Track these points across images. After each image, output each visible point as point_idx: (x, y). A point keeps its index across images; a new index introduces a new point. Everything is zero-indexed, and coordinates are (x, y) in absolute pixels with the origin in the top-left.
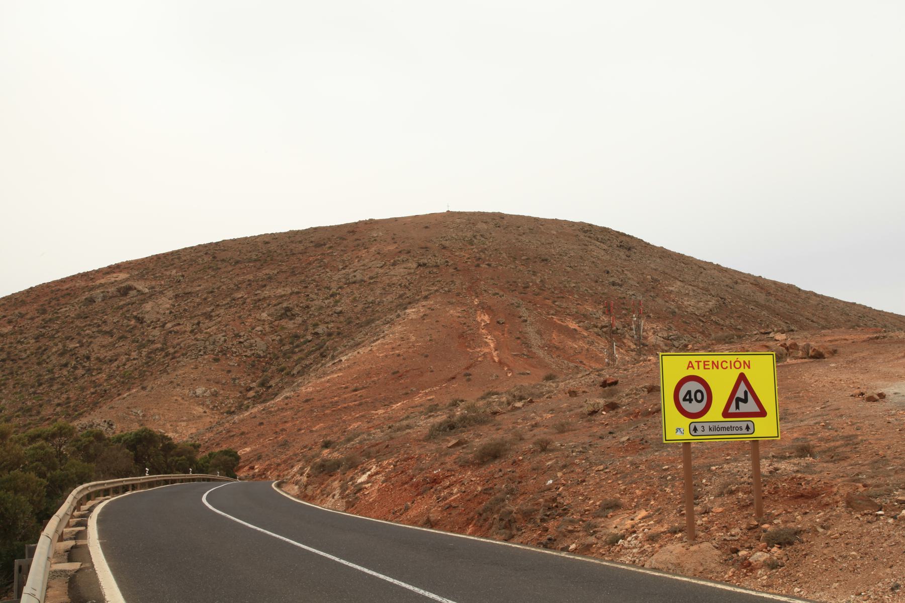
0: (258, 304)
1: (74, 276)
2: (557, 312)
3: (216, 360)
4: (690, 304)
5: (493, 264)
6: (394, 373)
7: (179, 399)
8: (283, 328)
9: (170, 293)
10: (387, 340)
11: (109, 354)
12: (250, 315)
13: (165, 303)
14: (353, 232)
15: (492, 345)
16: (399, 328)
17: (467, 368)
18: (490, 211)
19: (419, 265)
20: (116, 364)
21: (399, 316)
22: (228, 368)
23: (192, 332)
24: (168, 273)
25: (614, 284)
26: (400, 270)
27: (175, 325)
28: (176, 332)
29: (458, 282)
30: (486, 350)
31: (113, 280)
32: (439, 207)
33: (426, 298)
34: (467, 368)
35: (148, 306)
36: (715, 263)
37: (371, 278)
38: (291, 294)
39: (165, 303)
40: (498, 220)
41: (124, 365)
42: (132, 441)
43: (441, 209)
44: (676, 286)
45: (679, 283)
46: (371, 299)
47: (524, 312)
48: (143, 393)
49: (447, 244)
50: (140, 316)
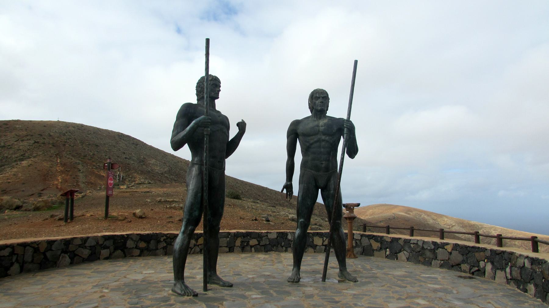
2: (97, 168)
4: (157, 169)
5: (72, 145)
6: (2, 191)
10: (7, 175)
14: (6, 124)
16: (15, 170)
17: (42, 190)
18: (338, 117)
19: (35, 142)
21: (17, 164)
25: (126, 158)
26: (25, 143)
29: (52, 152)
30: (56, 183)
32: (53, 118)
33: (35, 157)
34: (42, 190)
37: (9, 146)
40: (81, 128)
42: (428, 224)
43: (55, 119)
44: (153, 161)
45: (154, 160)
46: (6, 155)
47: (80, 167)
49: (52, 134)
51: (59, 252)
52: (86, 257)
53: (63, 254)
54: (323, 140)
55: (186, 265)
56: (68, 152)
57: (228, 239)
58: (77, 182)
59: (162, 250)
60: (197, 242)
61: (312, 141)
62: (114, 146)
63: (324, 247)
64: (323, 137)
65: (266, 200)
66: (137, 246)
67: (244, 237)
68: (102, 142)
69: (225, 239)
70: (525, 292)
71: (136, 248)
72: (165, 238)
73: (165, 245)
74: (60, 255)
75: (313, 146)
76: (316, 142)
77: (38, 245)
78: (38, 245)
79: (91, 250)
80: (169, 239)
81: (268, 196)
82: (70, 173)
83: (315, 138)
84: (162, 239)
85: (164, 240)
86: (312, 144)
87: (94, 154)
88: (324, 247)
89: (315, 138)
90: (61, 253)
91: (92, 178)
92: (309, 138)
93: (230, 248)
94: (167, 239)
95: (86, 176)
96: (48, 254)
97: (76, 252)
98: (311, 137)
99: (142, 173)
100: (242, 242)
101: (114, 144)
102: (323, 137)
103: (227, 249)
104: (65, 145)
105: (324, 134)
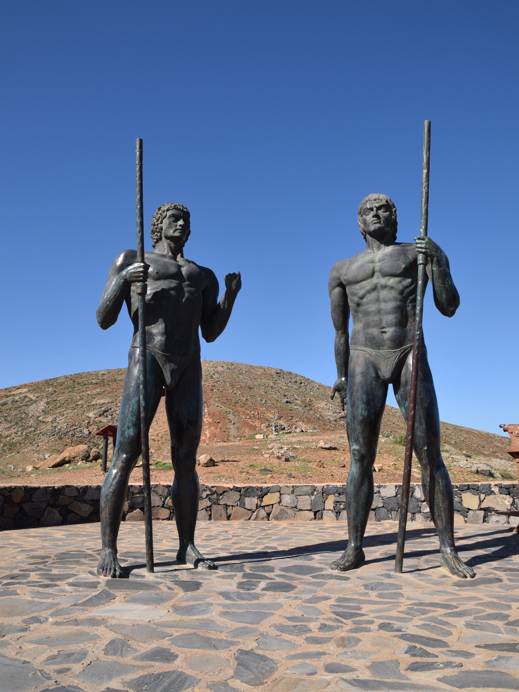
0: (90, 407)
1: (431, 382)
3: (61, 438)
5: (221, 389)
7: (36, 460)
8: (101, 422)
9: (45, 400)
11: (7, 433)
12: (84, 414)
13: (42, 405)
15: (208, 435)
20: (9, 438)
22: (66, 443)
23: (52, 422)
24: (47, 389)
27: (44, 418)
28: (43, 422)
31: (20, 392)
35: (31, 408)
36: (397, 235)
38: (108, 403)
39: (42, 405)
41: (13, 439)
47: (231, 417)
48: (18, 455)
50: (27, 412)
51: (44, 505)
52: (86, 515)
53: (50, 509)
54: (384, 287)
55: (196, 532)
56: (217, 399)
57: (313, 497)
58: (229, 436)
59: (204, 511)
60: (262, 502)
61: (361, 292)
62: (272, 387)
63: (482, 513)
64: (383, 281)
65: (494, 452)
66: (164, 502)
67: (340, 494)
68: (256, 383)
69: (307, 497)
70: (198, 588)
71: (163, 506)
72: (208, 492)
73: (209, 504)
74: (45, 510)
75: (365, 300)
76: (369, 292)
77: (10, 492)
78: (10, 492)
79: (93, 505)
80: (215, 495)
81: (497, 447)
82: (220, 425)
83: (367, 285)
84: (204, 495)
85: (207, 495)
86: (362, 298)
87: (247, 400)
88: (482, 513)
89: (367, 285)
90: (47, 506)
91: (246, 431)
92: (357, 286)
93: (315, 513)
94: (212, 494)
95: (238, 429)
96: (26, 506)
97: (69, 508)
98: (360, 284)
99: (309, 421)
100: (336, 502)
101: (271, 384)
102: (383, 281)
103: (311, 515)
104: (212, 390)
105: (385, 275)
